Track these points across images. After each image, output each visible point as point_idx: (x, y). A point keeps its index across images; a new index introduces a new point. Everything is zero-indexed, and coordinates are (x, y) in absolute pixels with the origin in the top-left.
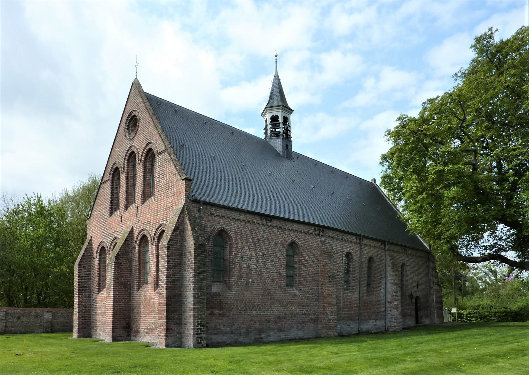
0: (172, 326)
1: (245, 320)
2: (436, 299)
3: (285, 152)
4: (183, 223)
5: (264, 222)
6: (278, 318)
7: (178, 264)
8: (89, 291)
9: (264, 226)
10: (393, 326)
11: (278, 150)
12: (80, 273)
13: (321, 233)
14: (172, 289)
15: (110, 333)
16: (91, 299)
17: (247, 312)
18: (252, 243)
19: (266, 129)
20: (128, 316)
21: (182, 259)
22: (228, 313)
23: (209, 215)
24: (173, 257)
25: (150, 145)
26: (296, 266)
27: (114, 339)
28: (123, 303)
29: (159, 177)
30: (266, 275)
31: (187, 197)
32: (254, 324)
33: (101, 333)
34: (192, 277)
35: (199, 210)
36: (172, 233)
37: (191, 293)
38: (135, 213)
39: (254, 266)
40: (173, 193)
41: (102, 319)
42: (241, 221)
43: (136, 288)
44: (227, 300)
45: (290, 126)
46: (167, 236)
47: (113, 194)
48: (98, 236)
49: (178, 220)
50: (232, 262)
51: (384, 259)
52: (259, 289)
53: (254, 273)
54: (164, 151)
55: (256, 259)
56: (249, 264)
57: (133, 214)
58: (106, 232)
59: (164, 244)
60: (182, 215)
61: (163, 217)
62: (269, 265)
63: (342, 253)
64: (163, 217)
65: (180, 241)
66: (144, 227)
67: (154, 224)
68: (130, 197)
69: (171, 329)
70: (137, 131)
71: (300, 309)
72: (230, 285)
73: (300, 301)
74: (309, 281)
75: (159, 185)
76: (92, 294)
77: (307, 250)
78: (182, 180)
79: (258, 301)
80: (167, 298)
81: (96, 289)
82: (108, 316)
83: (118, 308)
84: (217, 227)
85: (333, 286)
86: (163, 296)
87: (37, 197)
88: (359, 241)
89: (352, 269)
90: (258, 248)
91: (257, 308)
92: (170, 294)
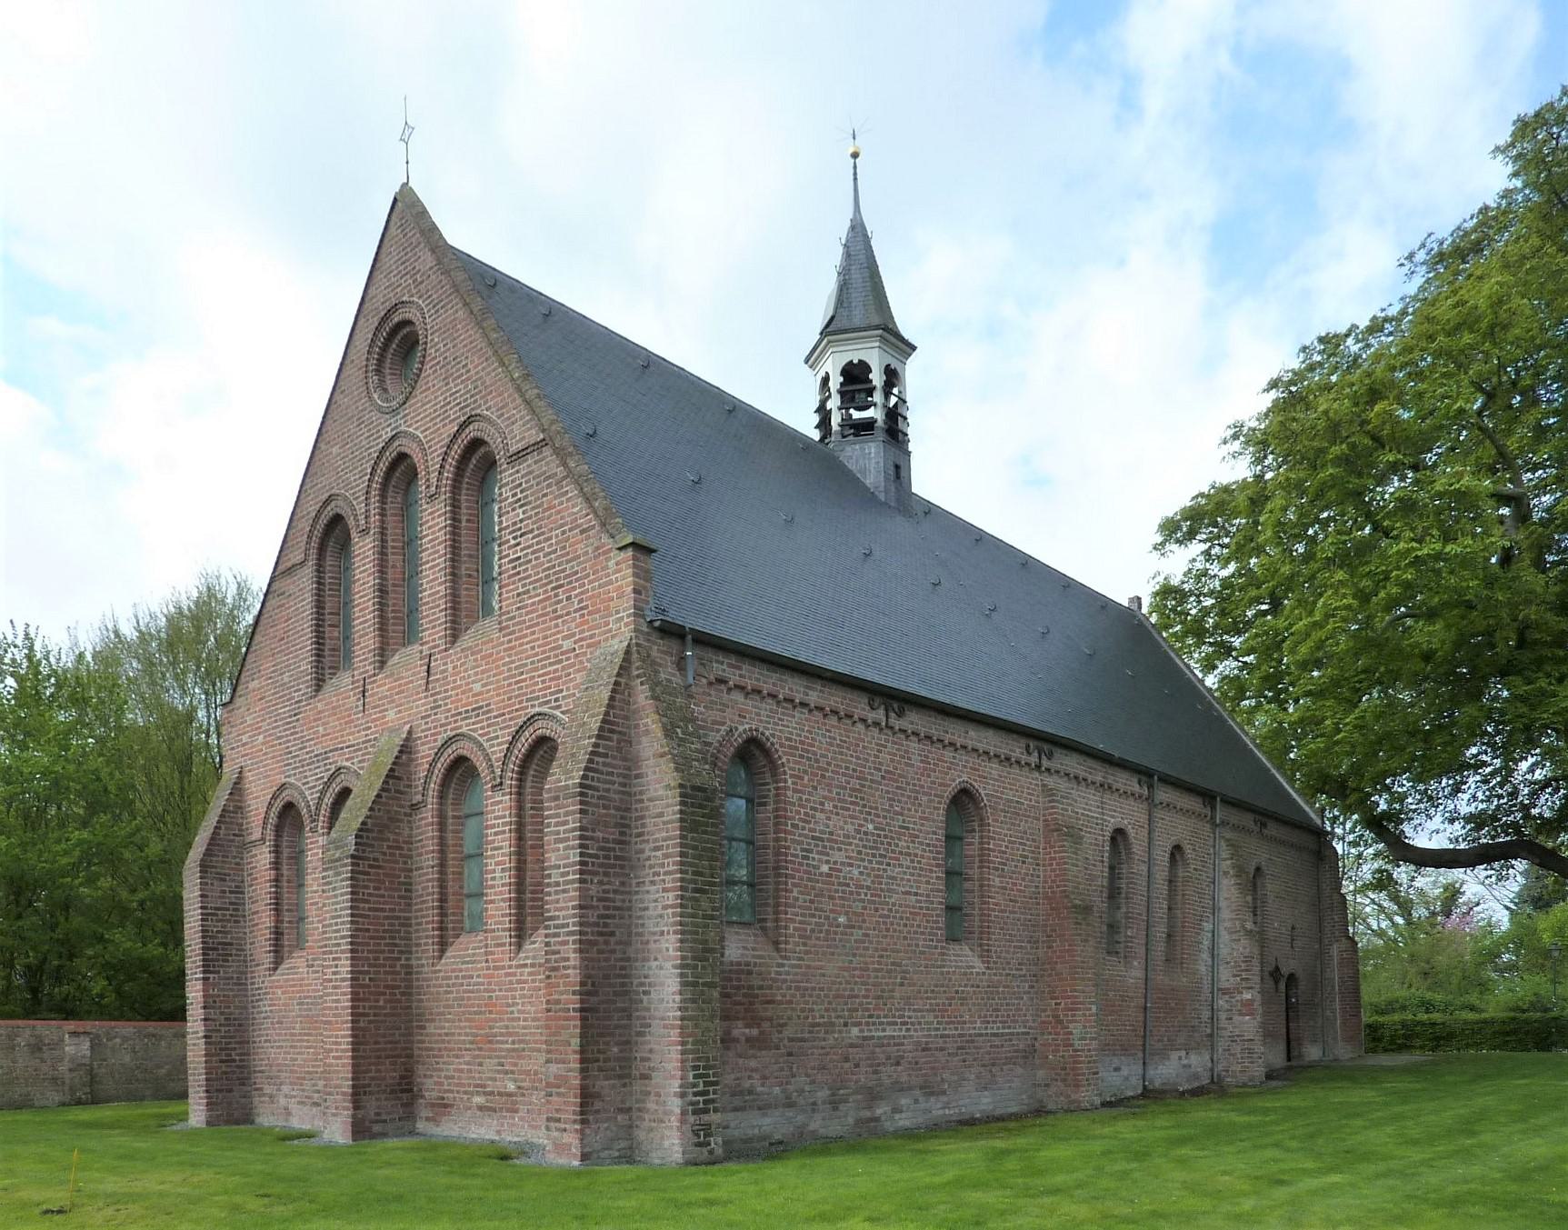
0: (603, 1085)
1: (828, 1057)
2: (1342, 982)
3: (893, 489)
4: (628, 710)
5: (880, 715)
6: (923, 1050)
7: (616, 858)
8: (239, 961)
9: (881, 730)
10: (1239, 1068)
11: (868, 482)
12: (206, 896)
13: (1045, 763)
14: (600, 952)
15: (345, 1108)
16: (246, 990)
17: (834, 1032)
18: (845, 788)
19: (822, 411)
20: (407, 1048)
21: (628, 839)
22: (775, 1037)
23: (710, 684)
24: (599, 834)
25: (476, 425)
26: (970, 872)
27: (361, 1130)
28: (386, 1001)
29: (518, 544)
30: (888, 904)
31: (639, 612)
32: (852, 1074)
33: (294, 1107)
34: (672, 906)
35: (681, 664)
36: (596, 745)
37: (668, 965)
38: (422, 678)
39: (850, 872)
40: (581, 601)
41: (296, 1059)
42: (810, 711)
43: (431, 949)
44: (770, 988)
45: (905, 402)
46: (573, 755)
47: (323, 614)
48: (268, 765)
49: (612, 698)
50: (786, 855)
51: (1212, 851)
52: (866, 949)
53: (851, 893)
54: (538, 446)
55: (857, 845)
56: (835, 863)
57: (412, 682)
58: (301, 749)
59: (567, 787)
60: (623, 681)
61: (540, 690)
62: (894, 865)
63: (1102, 830)
64: (540, 690)
65: (619, 775)
66: (461, 727)
67: (504, 714)
68: (394, 624)
69: (598, 1096)
70: (418, 376)
71: (985, 1016)
72: (780, 935)
73: (986, 992)
74: (1012, 924)
75: (519, 573)
76: (252, 972)
77: (1005, 817)
78: (620, 549)
79: (863, 993)
80: (582, 984)
81: (266, 952)
82: (331, 1050)
83: (370, 1022)
84: (737, 729)
85: (1086, 941)
86: (568, 976)
87: (21, 636)
88: (1146, 792)
89: (1128, 884)
90: (864, 806)
91: (863, 1017)
92: (593, 968)
